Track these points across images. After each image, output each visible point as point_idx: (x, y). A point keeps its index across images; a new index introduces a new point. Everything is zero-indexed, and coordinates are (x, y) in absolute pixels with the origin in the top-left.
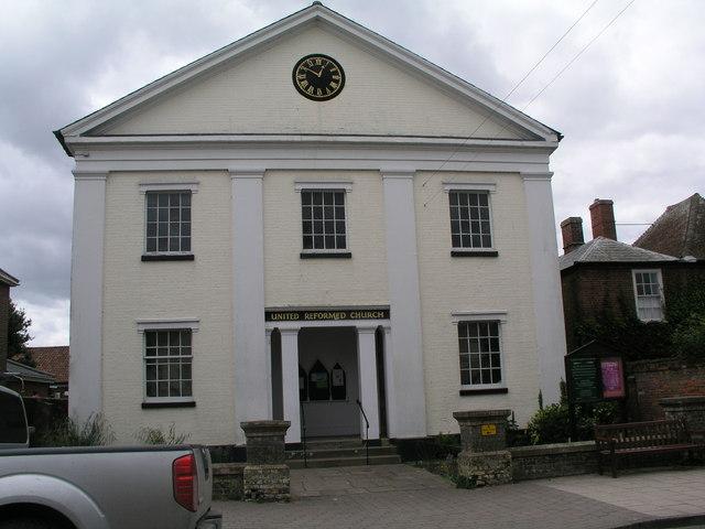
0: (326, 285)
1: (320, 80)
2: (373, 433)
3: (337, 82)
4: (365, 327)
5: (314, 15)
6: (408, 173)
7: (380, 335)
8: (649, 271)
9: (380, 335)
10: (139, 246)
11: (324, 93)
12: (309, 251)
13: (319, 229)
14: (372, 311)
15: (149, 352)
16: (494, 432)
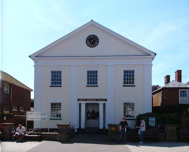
0: (92, 93)
1: (92, 41)
2: (150, 120)
3: (97, 42)
4: (101, 103)
5: (91, 24)
6: (112, 66)
7: (104, 105)
8: (186, 90)
9: (104, 105)
10: (50, 84)
11: (93, 45)
12: (125, 85)
13: (91, 80)
14: (103, 99)
15: (52, 108)
16: (114, 130)
